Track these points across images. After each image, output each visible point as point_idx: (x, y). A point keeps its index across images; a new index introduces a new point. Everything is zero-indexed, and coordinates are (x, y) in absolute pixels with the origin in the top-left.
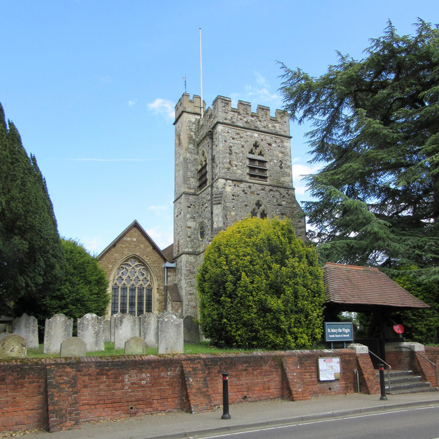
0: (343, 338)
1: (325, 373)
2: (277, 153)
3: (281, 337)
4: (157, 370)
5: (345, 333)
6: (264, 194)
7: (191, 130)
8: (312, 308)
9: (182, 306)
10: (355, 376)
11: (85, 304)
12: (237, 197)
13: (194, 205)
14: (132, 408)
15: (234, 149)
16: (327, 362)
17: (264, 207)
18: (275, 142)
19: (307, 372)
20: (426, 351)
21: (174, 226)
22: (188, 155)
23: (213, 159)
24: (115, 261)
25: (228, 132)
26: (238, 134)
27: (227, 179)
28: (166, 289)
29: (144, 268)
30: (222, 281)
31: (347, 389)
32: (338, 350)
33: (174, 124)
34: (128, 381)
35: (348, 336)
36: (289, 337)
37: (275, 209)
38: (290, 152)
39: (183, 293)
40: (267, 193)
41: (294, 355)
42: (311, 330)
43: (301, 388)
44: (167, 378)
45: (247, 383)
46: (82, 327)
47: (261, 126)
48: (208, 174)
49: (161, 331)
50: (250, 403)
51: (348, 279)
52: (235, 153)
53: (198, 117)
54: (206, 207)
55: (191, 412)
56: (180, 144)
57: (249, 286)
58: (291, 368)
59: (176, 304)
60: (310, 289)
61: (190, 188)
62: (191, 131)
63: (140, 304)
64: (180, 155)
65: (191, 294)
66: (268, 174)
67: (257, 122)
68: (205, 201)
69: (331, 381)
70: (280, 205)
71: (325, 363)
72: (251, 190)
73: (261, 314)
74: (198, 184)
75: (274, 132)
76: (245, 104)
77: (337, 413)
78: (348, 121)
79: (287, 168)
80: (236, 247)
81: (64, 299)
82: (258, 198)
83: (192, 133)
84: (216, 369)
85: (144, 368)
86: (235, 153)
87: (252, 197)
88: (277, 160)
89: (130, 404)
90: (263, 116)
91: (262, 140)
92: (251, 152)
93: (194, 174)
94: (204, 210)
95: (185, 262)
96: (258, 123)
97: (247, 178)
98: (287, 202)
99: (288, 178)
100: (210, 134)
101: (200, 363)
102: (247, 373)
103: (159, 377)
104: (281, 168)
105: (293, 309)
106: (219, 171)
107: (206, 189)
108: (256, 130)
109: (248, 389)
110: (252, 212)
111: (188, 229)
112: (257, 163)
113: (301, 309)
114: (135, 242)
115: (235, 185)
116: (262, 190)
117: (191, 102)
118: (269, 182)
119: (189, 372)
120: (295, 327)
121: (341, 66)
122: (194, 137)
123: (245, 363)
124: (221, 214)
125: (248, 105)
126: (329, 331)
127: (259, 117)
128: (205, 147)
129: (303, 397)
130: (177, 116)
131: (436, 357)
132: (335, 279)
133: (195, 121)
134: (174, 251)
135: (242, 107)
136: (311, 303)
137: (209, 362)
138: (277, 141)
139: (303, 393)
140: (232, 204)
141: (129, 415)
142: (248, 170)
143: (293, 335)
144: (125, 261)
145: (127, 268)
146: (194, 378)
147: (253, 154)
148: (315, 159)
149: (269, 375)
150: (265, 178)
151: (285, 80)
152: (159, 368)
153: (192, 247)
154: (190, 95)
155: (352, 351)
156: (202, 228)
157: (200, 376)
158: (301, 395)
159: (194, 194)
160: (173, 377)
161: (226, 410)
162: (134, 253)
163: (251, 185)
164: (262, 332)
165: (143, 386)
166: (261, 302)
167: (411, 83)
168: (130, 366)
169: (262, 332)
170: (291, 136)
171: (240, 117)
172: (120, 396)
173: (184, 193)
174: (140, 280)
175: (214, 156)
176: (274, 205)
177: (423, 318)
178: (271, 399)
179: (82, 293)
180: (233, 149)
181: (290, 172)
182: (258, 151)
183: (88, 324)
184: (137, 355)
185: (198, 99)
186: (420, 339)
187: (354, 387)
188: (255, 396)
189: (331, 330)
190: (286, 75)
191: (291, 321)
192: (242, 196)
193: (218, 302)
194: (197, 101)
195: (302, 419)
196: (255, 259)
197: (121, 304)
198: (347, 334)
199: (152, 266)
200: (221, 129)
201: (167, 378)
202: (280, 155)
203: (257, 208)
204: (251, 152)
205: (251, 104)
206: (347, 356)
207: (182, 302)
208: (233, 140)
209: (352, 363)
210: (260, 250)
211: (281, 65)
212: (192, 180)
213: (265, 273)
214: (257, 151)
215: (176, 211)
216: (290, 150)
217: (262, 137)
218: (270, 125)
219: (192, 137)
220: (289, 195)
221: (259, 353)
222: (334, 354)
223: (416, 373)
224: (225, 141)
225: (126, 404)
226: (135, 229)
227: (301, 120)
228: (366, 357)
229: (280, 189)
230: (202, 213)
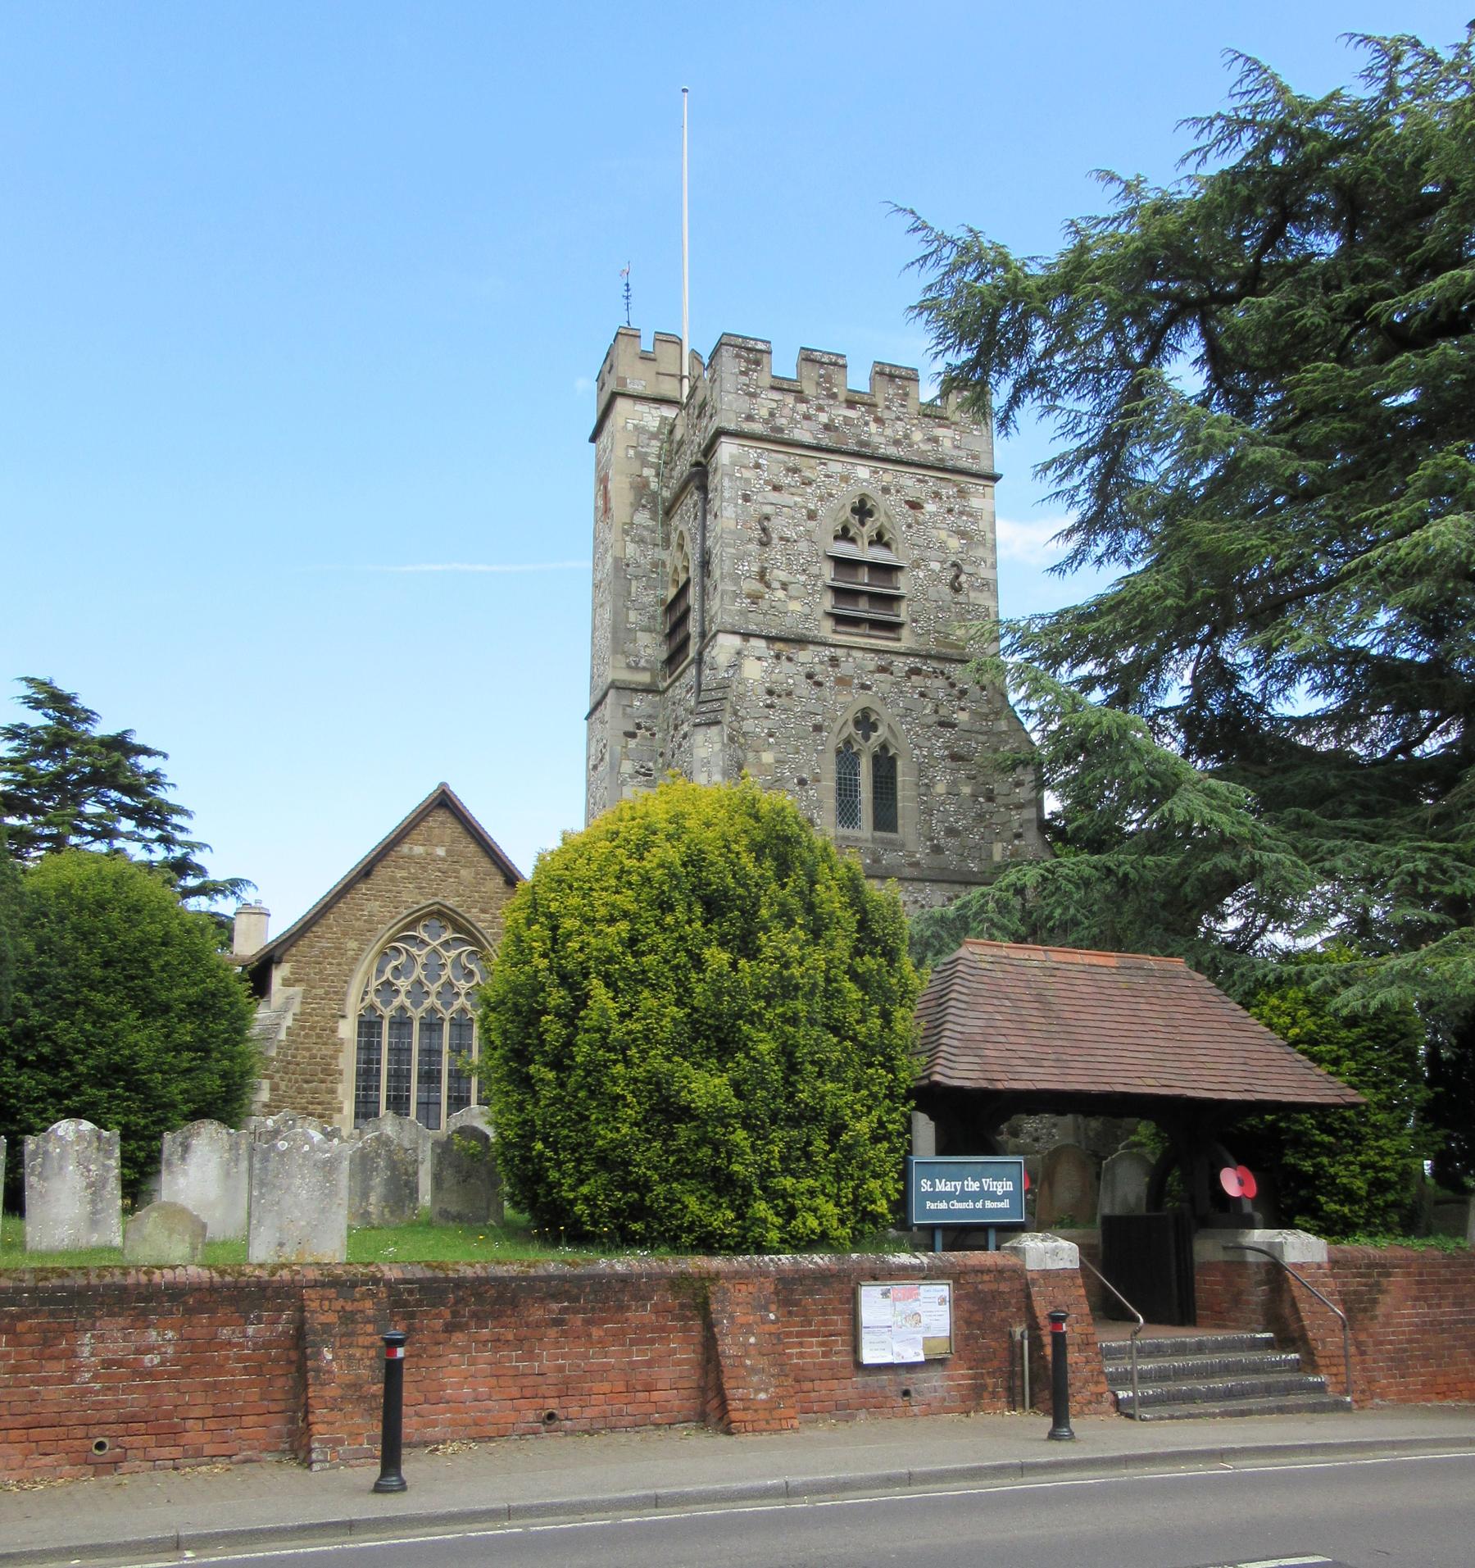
0: (984, 1212)
1: (886, 1337)
2: (943, 535)
3: (731, 1207)
4: (204, 1318)
5: (993, 1197)
6: (885, 687)
7: (643, 459)
8: (858, 1107)
10: (1014, 1350)
11: (144, 1083)
12: (784, 700)
13: (648, 729)
14: (100, 1446)
15: (778, 526)
16: (895, 1300)
19: (812, 1334)
20: (1334, 1263)
21: (588, 801)
22: (631, 549)
23: (705, 564)
24: (368, 926)
25: (758, 466)
27: (746, 636)
29: (473, 952)
30: (532, 1010)
31: (981, 1397)
32: (954, 1257)
33: (594, 438)
34: (92, 1355)
35: (1005, 1204)
36: (761, 1208)
37: (929, 739)
38: (993, 531)
40: (897, 683)
41: (762, 1273)
42: (851, 1184)
43: (766, 1391)
45: (561, 1369)
46: (42, 1165)
47: (882, 440)
50: (569, 1439)
51: (1040, 998)
52: (782, 539)
53: (670, 412)
55: (308, 1464)
56: (607, 510)
57: (616, 1026)
58: (742, 1320)
60: (853, 1039)
61: (636, 668)
62: (645, 463)
64: (606, 551)
66: (903, 612)
67: (867, 424)
68: (681, 712)
69: (911, 1367)
71: (888, 1301)
72: (839, 672)
73: (659, 1125)
75: (931, 459)
76: (825, 359)
77: (805, 1484)
79: (980, 589)
80: (591, 889)
81: (70, 1066)
82: (863, 700)
83: (649, 472)
84: (439, 1316)
85: (154, 1311)
86: (782, 539)
87: (841, 699)
88: (942, 562)
89: (95, 1430)
90: (891, 401)
91: (886, 490)
92: (844, 535)
93: (653, 617)
94: (680, 746)
96: (873, 427)
97: (826, 629)
98: (973, 713)
100: (696, 473)
101: (374, 1295)
102: (564, 1334)
103: (212, 1342)
104: (956, 588)
105: (779, 1110)
106: (724, 607)
107: (684, 671)
108: (864, 453)
109: (565, 1391)
110: (839, 752)
112: (864, 576)
113: (813, 1109)
114: (443, 860)
115: (778, 657)
116: (882, 670)
117: (645, 357)
118: (906, 640)
119: (327, 1328)
120: (787, 1171)
121: (1131, 213)
122: (654, 486)
123: (555, 1297)
124: (719, 762)
125: (835, 364)
126: (926, 1185)
127: (875, 406)
128: (684, 522)
129: (771, 1421)
130: (602, 407)
131: (1378, 1284)
132: (981, 1000)
133: (659, 428)
135: (814, 372)
136: (857, 1088)
137: (411, 1292)
138: (944, 492)
139: (772, 1406)
140: (766, 723)
141: (91, 1469)
142: (828, 602)
143: (780, 1202)
144: (407, 927)
145: (414, 951)
146: (341, 1347)
147: (853, 540)
148: (1075, 556)
149: (652, 1341)
150: (898, 625)
151: (932, 275)
152: (213, 1311)
154: (642, 333)
155: (1013, 1260)
157: (367, 1341)
158: (762, 1414)
159: (648, 690)
160: (267, 1345)
161: (391, 1460)
162: (437, 899)
163: (840, 652)
164: (660, 1189)
165: (150, 1373)
166: (656, 1083)
167: (1367, 265)
168: (102, 1304)
169: (660, 1189)
170: (997, 471)
171: (802, 407)
172: (58, 1404)
173: (614, 685)
174: (458, 994)
176: (922, 726)
177: (1358, 1139)
178: (658, 1425)
179: (130, 1046)
181: (990, 603)
182: (869, 529)
183: (62, 1156)
184: (138, 1269)
185: (673, 348)
186: (1344, 1216)
187: (1010, 1391)
188: (589, 1412)
189: (933, 1185)
191: (770, 1152)
192: (805, 693)
193: (526, 1083)
195: (657, 1502)
196: (644, 931)
197: (389, 1076)
198: (1000, 1199)
200: (732, 456)
201: (241, 1346)
202: (954, 543)
203: (859, 738)
204: (844, 535)
205: (848, 361)
206: (986, 1278)
208: (776, 494)
209: (1007, 1305)
210: (663, 902)
211: (909, 220)
212: (644, 638)
213: (679, 982)
214: (865, 530)
215: (593, 750)
217: (887, 478)
218: (917, 436)
219: (646, 485)
220: (983, 688)
221: (624, 1263)
222: (930, 1268)
223: (1285, 1341)
224: (746, 498)
225: (80, 1432)
226: (441, 816)
228: (1068, 1282)
229: (948, 668)
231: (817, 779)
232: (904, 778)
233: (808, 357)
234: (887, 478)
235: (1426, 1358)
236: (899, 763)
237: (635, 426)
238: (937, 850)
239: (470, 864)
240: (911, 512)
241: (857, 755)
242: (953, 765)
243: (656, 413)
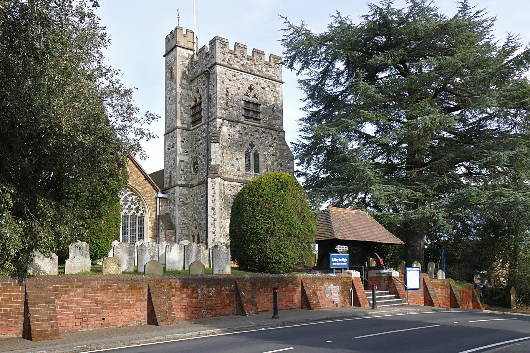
5: (343, 262)
9: (175, 234)
13: (187, 140)
17: (257, 148)
18: (269, 86)
21: (165, 158)
25: (225, 74)
26: (235, 76)
28: (158, 218)
35: (346, 264)
39: (177, 222)
44: (226, 291)
48: (203, 111)
49: (215, 257)
53: (191, 53)
54: (201, 144)
63: (133, 230)
65: (184, 224)
76: (242, 47)
78: (339, 74)
86: (231, 94)
94: (198, 146)
95: (179, 194)
98: (277, 144)
99: (279, 121)
103: (221, 291)
111: (181, 163)
116: (256, 131)
117: (184, 36)
122: (187, 73)
134: (165, 183)
138: (270, 85)
142: (243, 112)
150: (260, 120)
153: (185, 180)
154: (183, 29)
156: (195, 163)
159: (187, 129)
160: (230, 291)
163: (246, 126)
165: (210, 297)
170: (283, 81)
171: (236, 59)
175: (211, 95)
182: (252, 94)
183: (145, 250)
190: (289, 30)
194: (190, 35)
198: (345, 263)
199: (144, 196)
201: (226, 291)
204: (246, 95)
207: (175, 230)
215: (167, 144)
216: (282, 95)
217: (257, 80)
218: (264, 70)
220: (280, 138)
224: (223, 82)
227: (299, 71)
229: (271, 131)
230: (195, 148)
231: (241, 159)
232: (261, 159)
233: (237, 45)
234: (257, 80)
235: (414, 296)
236: (260, 155)
237: (182, 55)
239: (135, 173)
240: (263, 90)
242: (273, 157)
243: (187, 52)
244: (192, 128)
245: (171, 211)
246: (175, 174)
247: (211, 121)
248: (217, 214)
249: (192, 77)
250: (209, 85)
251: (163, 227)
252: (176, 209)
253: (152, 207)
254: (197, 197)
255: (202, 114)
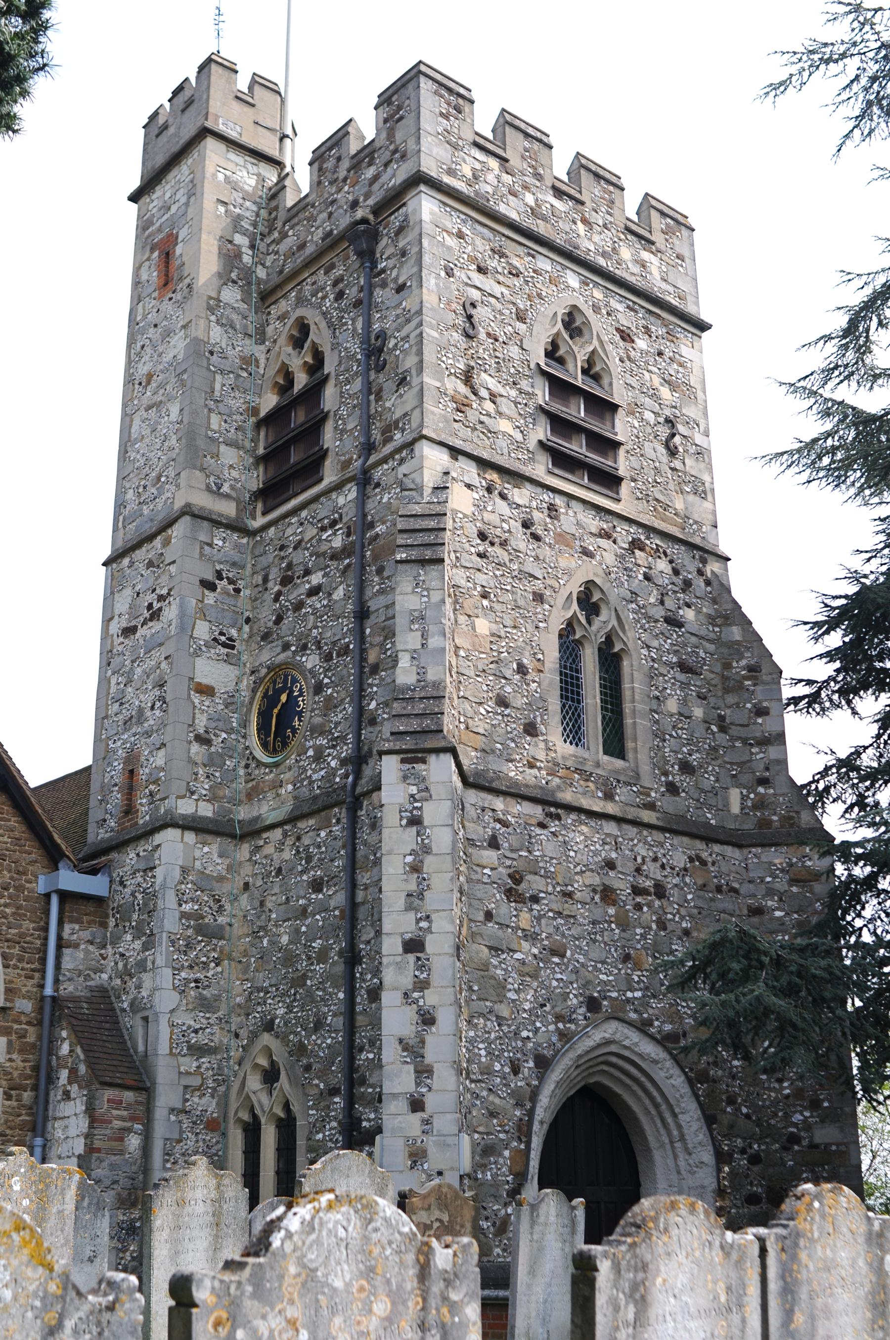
2: (657, 381)
13: (231, 581)
17: (614, 622)
21: (104, 682)
22: (216, 334)
27: (455, 452)
54: (314, 591)
59: (117, 1103)
61: (216, 491)
65: (197, 1051)
70: (674, 622)
74: (254, 480)
82: (587, 571)
83: (240, 240)
86: (489, 335)
94: (299, 606)
96: (581, 228)
97: (540, 468)
104: (672, 452)
111: (196, 699)
115: (489, 490)
116: (605, 535)
122: (247, 259)
125: (540, 141)
127: (582, 203)
134: (95, 814)
138: (653, 329)
142: (541, 431)
159: (235, 527)
163: (559, 501)
171: (506, 178)
173: (188, 511)
175: (382, 336)
180: (481, 313)
212: (229, 456)
215: (122, 604)
218: (626, 253)
219: (238, 255)
224: (449, 273)
230: (279, 620)
236: (625, 663)
238: (672, 789)
241: (579, 643)
242: (682, 677)
243: (254, 170)
244: (259, 522)
245: (126, 974)
246: (160, 759)
247: (385, 460)
248: (435, 980)
249: (266, 282)
250: (370, 289)
251: (73, 1071)
252: (160, 961)
253: (16, 951)
254: (285, 889)
255: (329, 437)
